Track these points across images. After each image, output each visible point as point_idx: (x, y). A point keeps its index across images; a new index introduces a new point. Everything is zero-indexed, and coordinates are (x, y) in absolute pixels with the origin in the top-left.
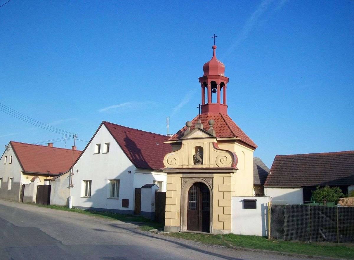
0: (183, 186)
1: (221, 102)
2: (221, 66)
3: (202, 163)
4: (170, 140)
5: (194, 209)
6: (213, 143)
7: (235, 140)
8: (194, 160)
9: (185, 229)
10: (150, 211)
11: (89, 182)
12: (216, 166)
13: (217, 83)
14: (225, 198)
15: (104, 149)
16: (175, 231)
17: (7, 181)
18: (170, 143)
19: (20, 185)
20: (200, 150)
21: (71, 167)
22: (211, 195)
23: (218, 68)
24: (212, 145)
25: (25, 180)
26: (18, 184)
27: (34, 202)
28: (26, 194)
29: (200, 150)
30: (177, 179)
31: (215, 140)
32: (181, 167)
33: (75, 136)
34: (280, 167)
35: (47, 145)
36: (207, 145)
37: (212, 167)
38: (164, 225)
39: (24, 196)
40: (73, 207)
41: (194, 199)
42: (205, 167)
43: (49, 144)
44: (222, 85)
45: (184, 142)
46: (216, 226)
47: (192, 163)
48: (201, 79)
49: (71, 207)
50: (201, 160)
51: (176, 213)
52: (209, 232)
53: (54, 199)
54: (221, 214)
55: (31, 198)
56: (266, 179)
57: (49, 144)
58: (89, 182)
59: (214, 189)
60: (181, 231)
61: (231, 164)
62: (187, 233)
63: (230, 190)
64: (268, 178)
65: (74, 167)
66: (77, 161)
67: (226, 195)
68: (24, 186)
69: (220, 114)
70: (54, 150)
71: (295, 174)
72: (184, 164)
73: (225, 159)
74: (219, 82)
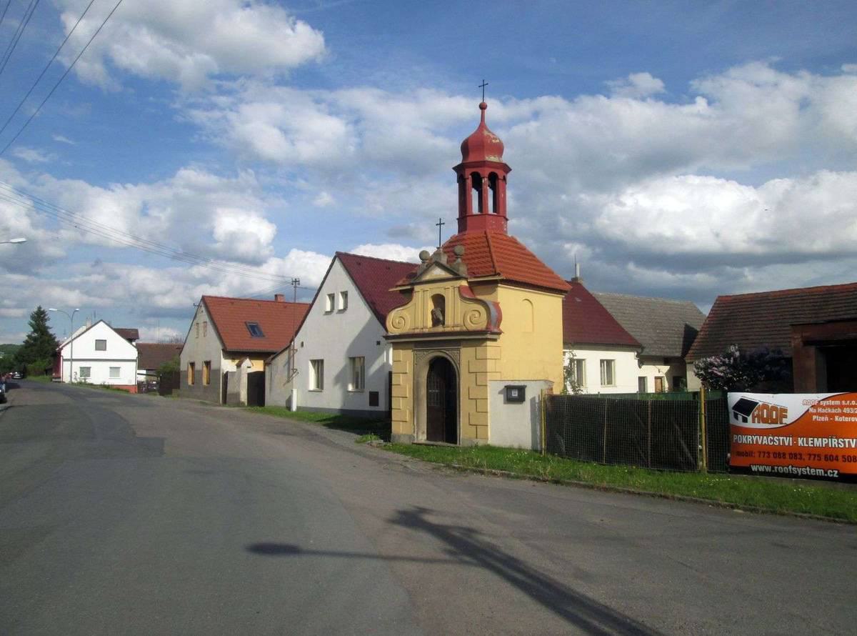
0: (415, 364)
1: (490, 210)
2: (491, 141)
3: (444, 324)
4: (400, 286)
5: (437, 404)
6: (459, 287)
7: (496, 280)
8: (433, 319)
9: (423, 438)
10: (384, 410)
11: (605, 363)
12: (464, 329)
13: (482, 176)
14: (478, 383)
15: (340, 304)
16: (406, 441)
17: (186, 369)
18: (400, 291)
19: (221, 372)
20: (439, 301)
21: (292, 340)
22: (458, 379)
23: (483, 146)
24: (457, 290)
25: (228, 365)
26: (218, 370)
27: (243, 403)
28: (230, 389)
29: (439, 301)
30: (407, 356)
31: (464, 283)
32: (411, 332)
33: (296, 281)
34: (724, 320)
35: (273, 299)
36: (450, 292)
37: (458, 329)
38: (391, 432)
39: (228, 393)
40: (298, 408)
41: (437, 387)
42: (447, 329)
43: (276, 296)
44: (493, 179)
45: (417, 288)
46: (465, 431)
47: (430, 323)
48: (457, 169)
49: (294, 408)
50: (441, 318)
51: (408, 411)
52: (456, 443)
53: (273, 396)
54: (473, 412)
55: (237, 395)
56: (691, 345)
57: (276, 296)
58: (318, 364)
59: (461, 368)
60: (415, 442)
61: (486, 324)
62: (426, 445)
63: (486, 369)
64: (695, 344)
65: (296, 340)
66: (300, 327)
67: (480, 375)
68: (226, 376)
69: (485, 233)
70: (285, 307)
71: (751, 333)
72: (416, 326)
73: (477, 315)
74: (485, 172)
